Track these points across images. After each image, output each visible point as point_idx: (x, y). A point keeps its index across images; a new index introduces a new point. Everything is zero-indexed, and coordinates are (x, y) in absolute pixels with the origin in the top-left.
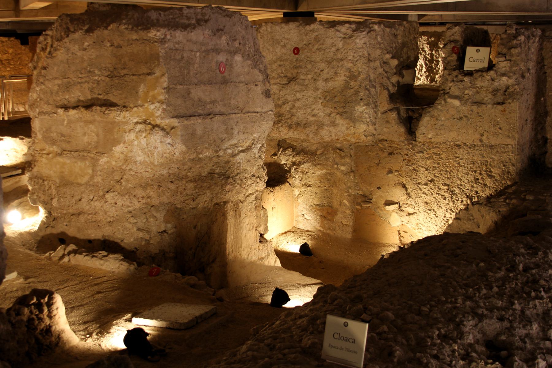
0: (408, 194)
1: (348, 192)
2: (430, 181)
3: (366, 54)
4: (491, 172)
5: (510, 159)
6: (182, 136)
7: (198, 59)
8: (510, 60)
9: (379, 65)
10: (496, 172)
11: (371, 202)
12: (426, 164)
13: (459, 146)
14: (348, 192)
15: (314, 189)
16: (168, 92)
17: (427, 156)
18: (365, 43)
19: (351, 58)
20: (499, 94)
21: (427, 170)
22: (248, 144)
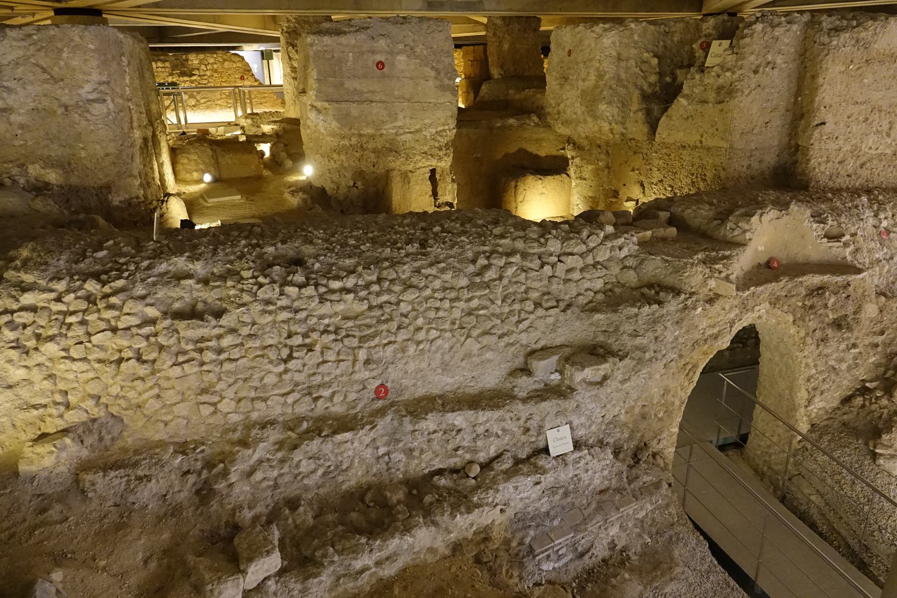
0: (644, 193)
1: (602, 186)
2: (660, 181)
3: (614, 54)
4: (705, 175)
5: (722, 163)
6: (334, 115)
7: (351, 59)
8: (737, 54)
9: (634, 64)
10: (709, 175)
11: (617, 198)
12: (658, 165)
13: (684, 147)
14: (602, 186)
15: (589, 182)
16: (318, 83)
17: (660, 156)
18: (613, 43)
19: (598, 57)
20: (723, 92)
21: (658, 170)
22: (417, 127)
